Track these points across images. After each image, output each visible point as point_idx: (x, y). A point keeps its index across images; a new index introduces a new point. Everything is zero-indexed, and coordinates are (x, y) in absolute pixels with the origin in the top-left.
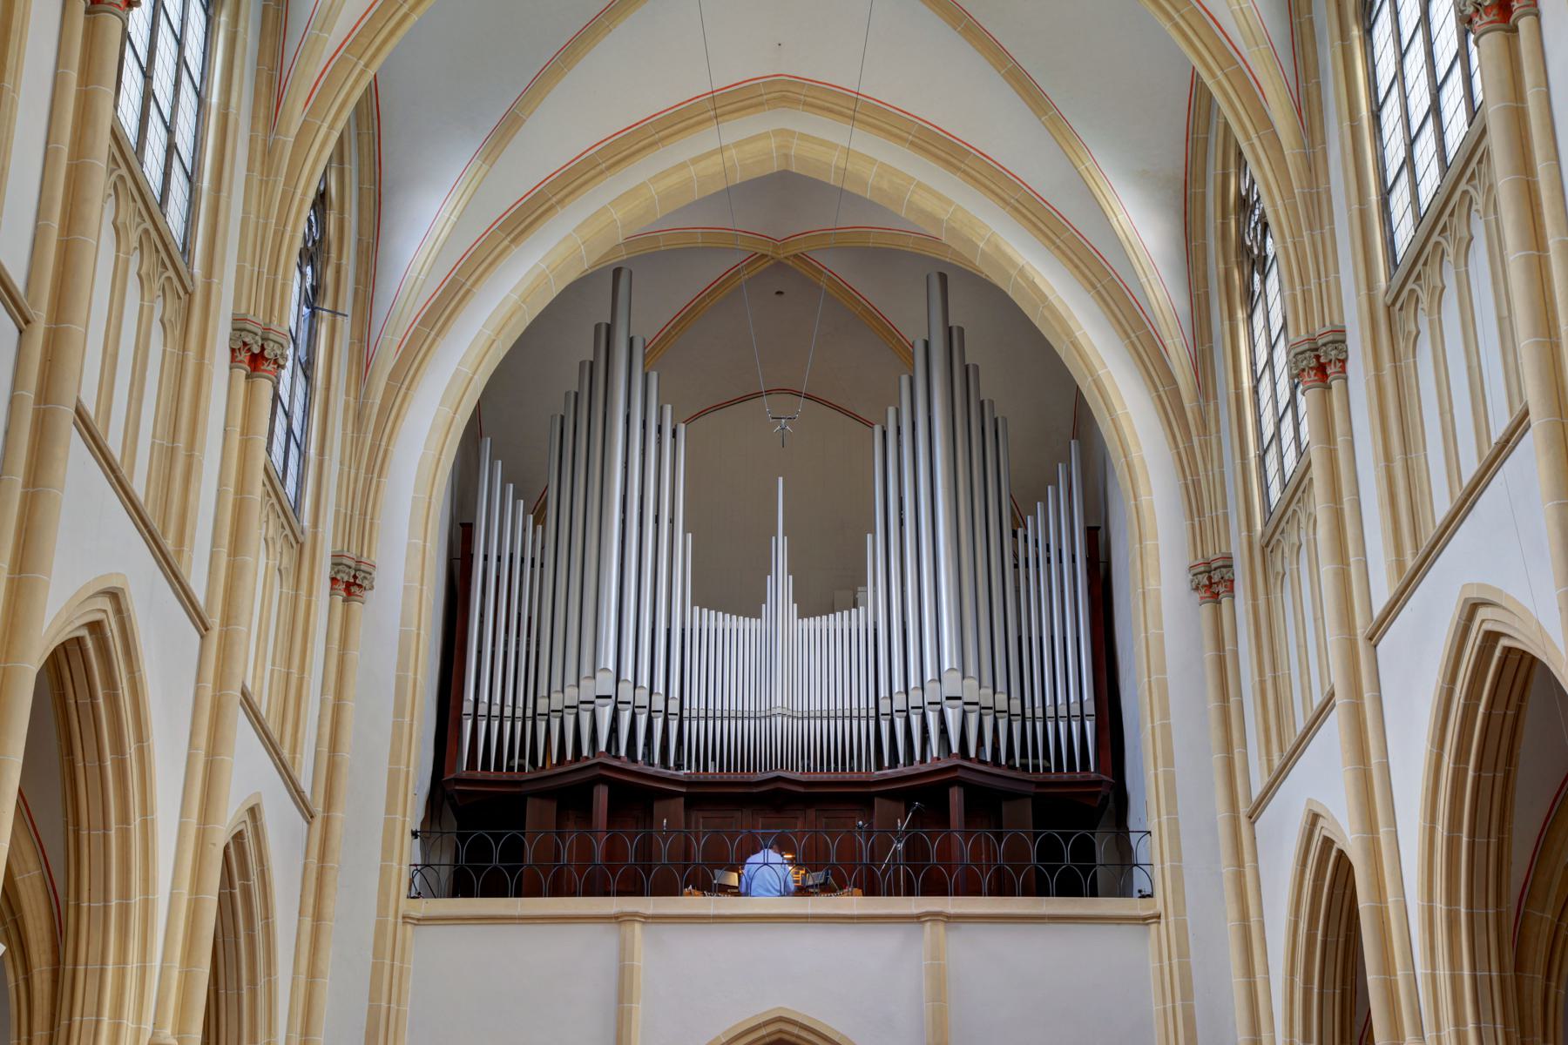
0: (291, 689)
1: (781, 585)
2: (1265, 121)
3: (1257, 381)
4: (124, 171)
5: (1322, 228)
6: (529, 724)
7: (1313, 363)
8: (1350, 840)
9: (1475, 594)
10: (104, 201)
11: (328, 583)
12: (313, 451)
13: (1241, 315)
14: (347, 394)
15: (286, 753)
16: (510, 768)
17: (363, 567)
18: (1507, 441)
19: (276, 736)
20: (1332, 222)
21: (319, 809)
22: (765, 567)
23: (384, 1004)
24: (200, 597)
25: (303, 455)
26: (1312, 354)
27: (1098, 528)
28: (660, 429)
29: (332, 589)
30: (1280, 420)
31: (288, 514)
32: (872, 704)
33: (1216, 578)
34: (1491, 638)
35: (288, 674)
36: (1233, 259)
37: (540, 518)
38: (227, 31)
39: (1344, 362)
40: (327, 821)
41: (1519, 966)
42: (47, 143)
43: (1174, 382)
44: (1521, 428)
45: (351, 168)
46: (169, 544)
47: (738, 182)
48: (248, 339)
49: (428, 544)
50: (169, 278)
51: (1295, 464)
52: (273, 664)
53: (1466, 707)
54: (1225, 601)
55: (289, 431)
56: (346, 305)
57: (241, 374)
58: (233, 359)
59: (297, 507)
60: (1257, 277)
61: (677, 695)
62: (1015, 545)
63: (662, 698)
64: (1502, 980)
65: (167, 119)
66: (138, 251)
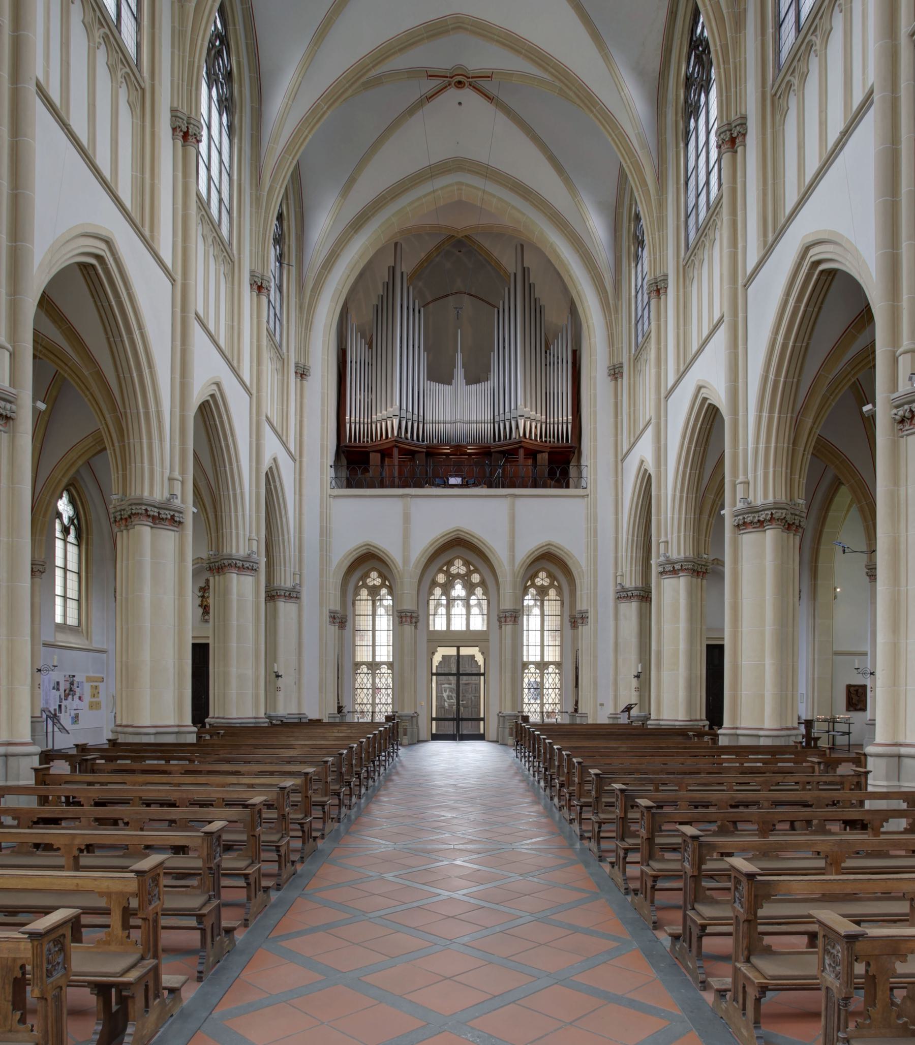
0: (284, 415)
1: (459, 373)
2: (644, 183)
3: (637, 293)
4: (203, 212)
5: (663, 231)
6: (369, 426)
7: (655, 288)
8: (652, 470)
9: (701, 383)
10: (197, 226)
11: (294, 374)
12: (285, 322)
13: (633, 265)
14: (296, 298)
15: (284, 439)
16: (364, 442)
17: (306, 367)
18: (717, 325)
19: (280, 433)
20: (667, 230)
21: (297, 458)
22: (454, 366)
23: (325, 525)
24: (248, 383)
25: (281, 324)
26: (655, 285)
27: (577, 350)
28: (414, 310)
29: (296, 376)
30: (644, 309)
31: (277, 348)
32: (492, 418)
33: (617, 371)
34: (705, 399)
35: (283, 409)
36: (631, 241)
37: (370, 347)
38: (238, 146)
39: (666, 288)
40: (301, 462)
41: (700, 514)
42: (173, 205)
43: (607, 292)
44: (841, 143)
45: (291, 202)
46: (235, 364)
47: (442, 204)
48: (256, 280)
49: (329, 358)
50: (225, 256)
51: (794, 41)
52: (277, 405)
53: (694, 425)
54: (619, 380)
55: (275, 314)
56: (293, 262)
57: (255, 294)
58: (251, 288)
59: (281, 345)
60: (640, 249)
61: (422, 415)
62: (546, 358)
63: (417, 416)
64: (694, 518)
65: (218, 188)
66: (212, 246)
